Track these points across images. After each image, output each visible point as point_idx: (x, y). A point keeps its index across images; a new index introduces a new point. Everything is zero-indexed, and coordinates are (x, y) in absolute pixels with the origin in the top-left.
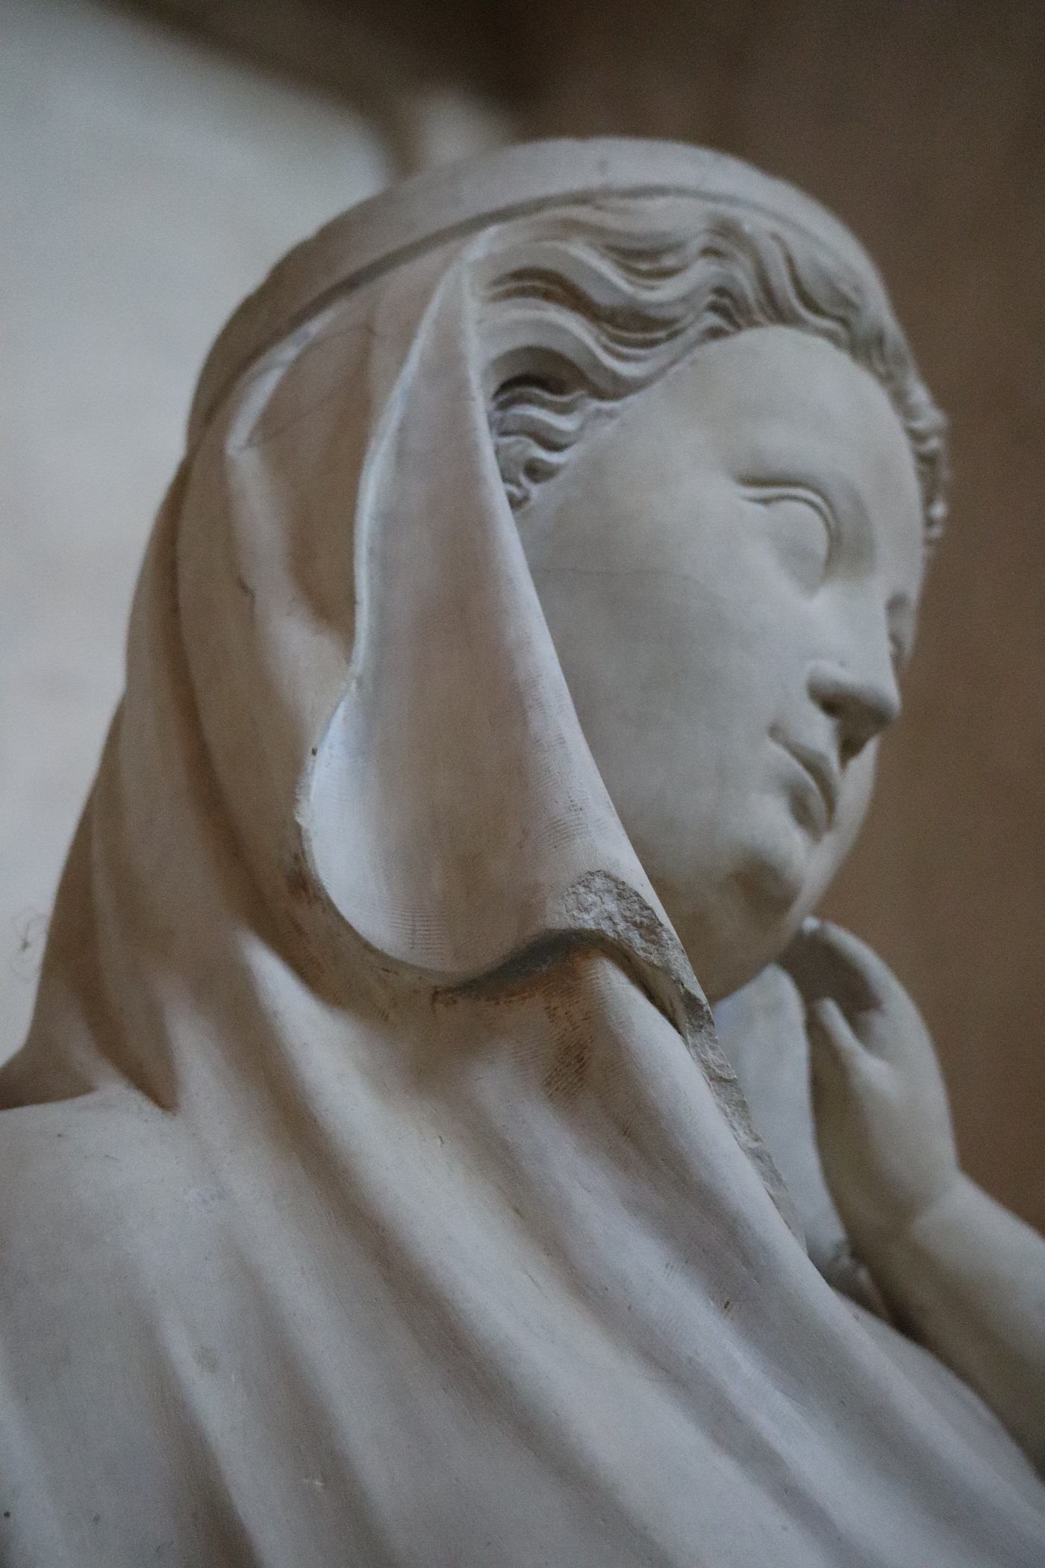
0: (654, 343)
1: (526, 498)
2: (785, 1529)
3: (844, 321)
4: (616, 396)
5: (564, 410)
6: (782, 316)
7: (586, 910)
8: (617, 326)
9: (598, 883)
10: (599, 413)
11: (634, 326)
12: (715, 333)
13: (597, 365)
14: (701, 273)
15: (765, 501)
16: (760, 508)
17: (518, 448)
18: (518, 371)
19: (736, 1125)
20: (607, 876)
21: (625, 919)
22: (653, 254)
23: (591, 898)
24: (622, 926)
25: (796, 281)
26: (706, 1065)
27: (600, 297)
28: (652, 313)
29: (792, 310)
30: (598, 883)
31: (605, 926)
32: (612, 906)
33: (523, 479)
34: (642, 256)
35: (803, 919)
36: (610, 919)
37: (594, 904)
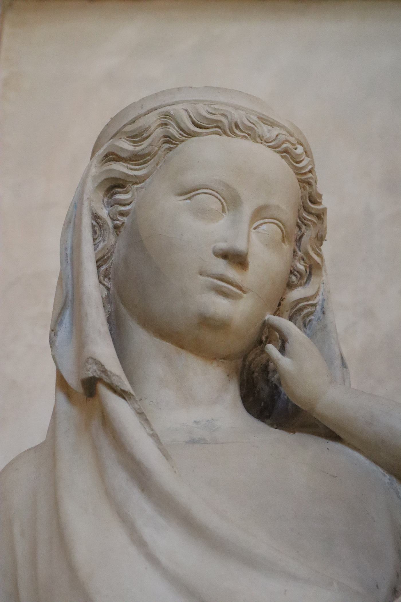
0: (148, 161)
1: (123, 223)
2: (146, 568)
3: (218, 127)
4: (144, 181)
5: (126, 192)
6: (190, 135)
7: (89, 371)
8: (133, 161)
9: (90, 360)
10: (137, 189)
11: (137, 159)
12: (170, 149)
13: (128, 175)
14: (159, 132)
15: (189, 198)
16: (188, 201)
17: (114, 209)
18: (107, 186)
19: (146, 427)
20: (92, 358)
21: (99, 370)
22: (141, 134)
23: (89, 366)
24: (99, 373)
25: (194, 123)
26: (134, 409)
27: (124, 155)
28: (141, 153)
29: (193, 131)
30: (90, 360)
31: (95, 374)
32: (95, 367)
33: (119, 218)
34: (136, 137)
35: (265, 315)
36: (95, 371)
37: (90, 368)
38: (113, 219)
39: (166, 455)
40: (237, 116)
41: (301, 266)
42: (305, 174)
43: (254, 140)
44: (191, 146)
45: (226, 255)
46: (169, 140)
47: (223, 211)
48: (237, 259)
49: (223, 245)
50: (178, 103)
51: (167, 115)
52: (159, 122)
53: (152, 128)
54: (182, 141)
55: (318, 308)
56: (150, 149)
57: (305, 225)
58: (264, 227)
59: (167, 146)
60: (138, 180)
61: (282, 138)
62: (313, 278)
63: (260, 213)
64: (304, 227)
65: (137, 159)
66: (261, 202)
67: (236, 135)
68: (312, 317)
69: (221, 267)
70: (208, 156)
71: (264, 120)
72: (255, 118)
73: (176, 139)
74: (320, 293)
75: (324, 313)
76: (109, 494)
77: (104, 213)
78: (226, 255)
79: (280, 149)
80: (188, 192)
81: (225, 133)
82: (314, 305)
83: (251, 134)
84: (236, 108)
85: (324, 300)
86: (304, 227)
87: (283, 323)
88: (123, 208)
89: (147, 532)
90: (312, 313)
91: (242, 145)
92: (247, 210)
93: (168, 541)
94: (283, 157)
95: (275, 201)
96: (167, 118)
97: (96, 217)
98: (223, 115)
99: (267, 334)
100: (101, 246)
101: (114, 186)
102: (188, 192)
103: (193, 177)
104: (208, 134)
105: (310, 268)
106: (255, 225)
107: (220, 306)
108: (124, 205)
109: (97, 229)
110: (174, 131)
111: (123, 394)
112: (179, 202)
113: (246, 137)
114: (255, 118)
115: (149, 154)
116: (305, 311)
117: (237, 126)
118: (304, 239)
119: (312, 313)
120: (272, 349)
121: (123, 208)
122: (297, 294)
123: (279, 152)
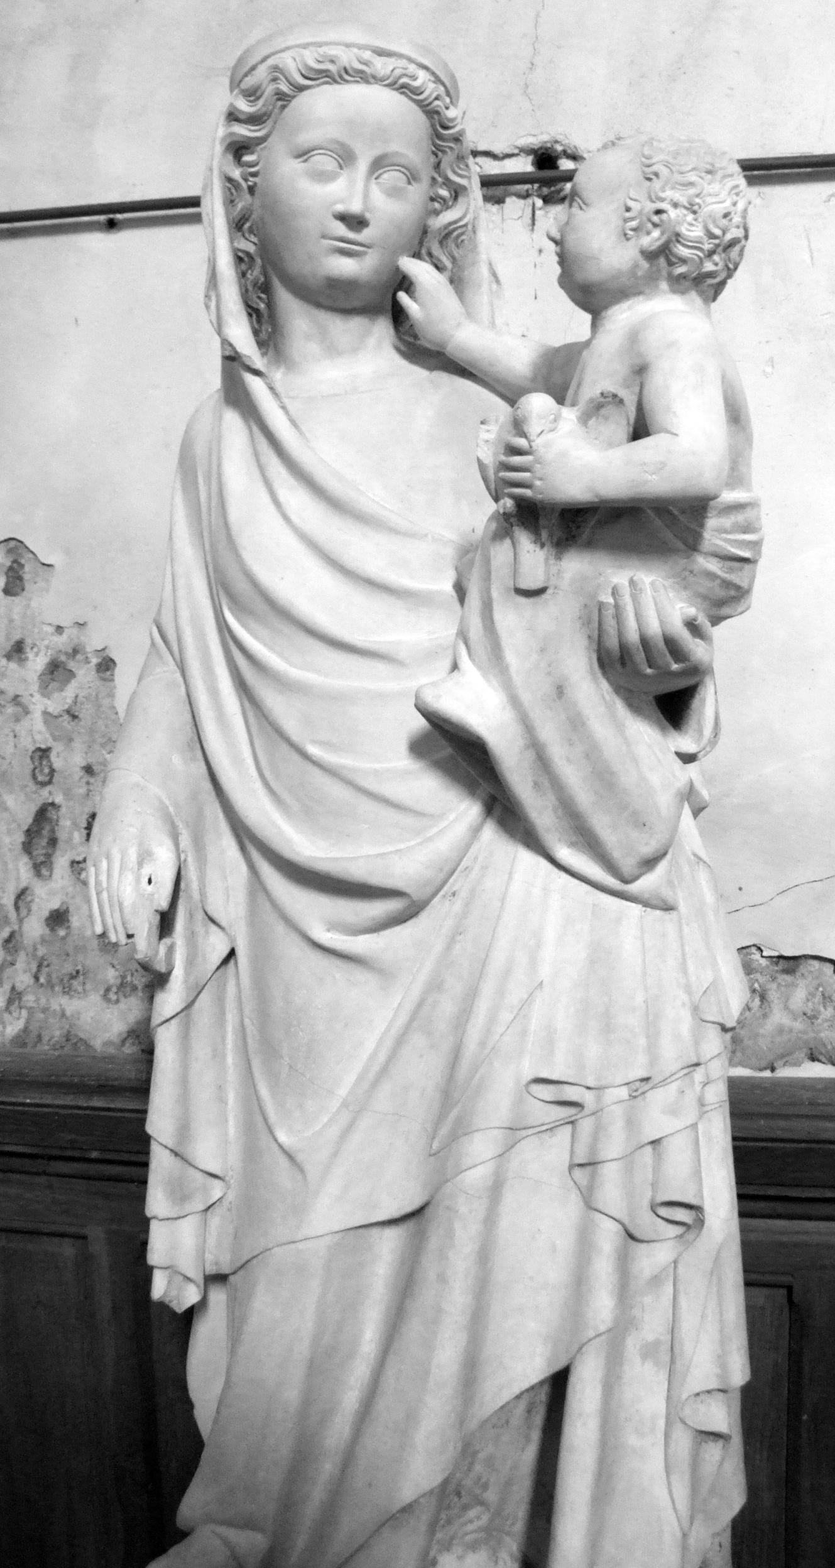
5: (252, 153)
6: (301, 89)
11: (254, 120)
13: (249, 138)
14: (270, 89)
15: (305, 161)
25: (303, 75)
27: (242, 117)
38: (246, 180)
39: (293, 423)
40: (347, 58)
41: (444, 193)
42: (430, 103)
43: (368, 82)
44: (303, 99)
45: (343, 218)
46: (283, 98)
47: (341, 167)
48: (356, 222)
49: (340, 208)
50: (288, 48)
51: (276, 68)
52: (270, 77)
53: (264, 86)
54: (294, 97)
55: (470, 227)
56: (264, 109)
57: (442, 151)
58: (385, 176)
59: (280, 103)
60: (263, 139)
61: (398, 72)
62: (460, 199)
63: (378, 164)
64: (440, 154)
65: (254, 120)
66: (377, 152)
67: (347, 81)
68: (463, 237)
69: (341, 229)
70: (323, 110)
71: (381, 53)
72: (367, 55)
73: (289, 96)
74: (471, 211)
75: (474, 232)
76: (256, 455)
77: (236, 174)
78: (343, 218)
79: (396, 86)
80: (303, 154)
81: (336, 82)
82: (465, 225)
83: (364, 78)
84: (348, 46)
85: (475, 218)
86: (440, 154)
87: (419, 270)
88: (253, 170)
89: (283, 494)
90: (462, 234)
91: (354, 92)
92: (363, 165)
93: (296, 498)
94: (402, 93)
95: (394, 147)
96: (277, 72)
97: (230, 180)
98: (332, 61)
99: (405, 283)
100: (240, 206)
101: (238, 149)
102: (303, 154)
103: (306, 138)
104: (318, 85)
105: (456, 192)
106: (376, 175)
107: (346, 267)
108: (253, 166)
109: (233, 191)
110: (284, 87)
111: (257, 373)
112: (297, 165)
113: (358, 82)
114: (367, 55)
115: (265, 114)
116: (455, 234)
117: (346, 72)
118: (443, 165)
119: (462, 234)
120: (402, 296)
121: (253, 170)
122: (448, 217)
123: (397, 89)
